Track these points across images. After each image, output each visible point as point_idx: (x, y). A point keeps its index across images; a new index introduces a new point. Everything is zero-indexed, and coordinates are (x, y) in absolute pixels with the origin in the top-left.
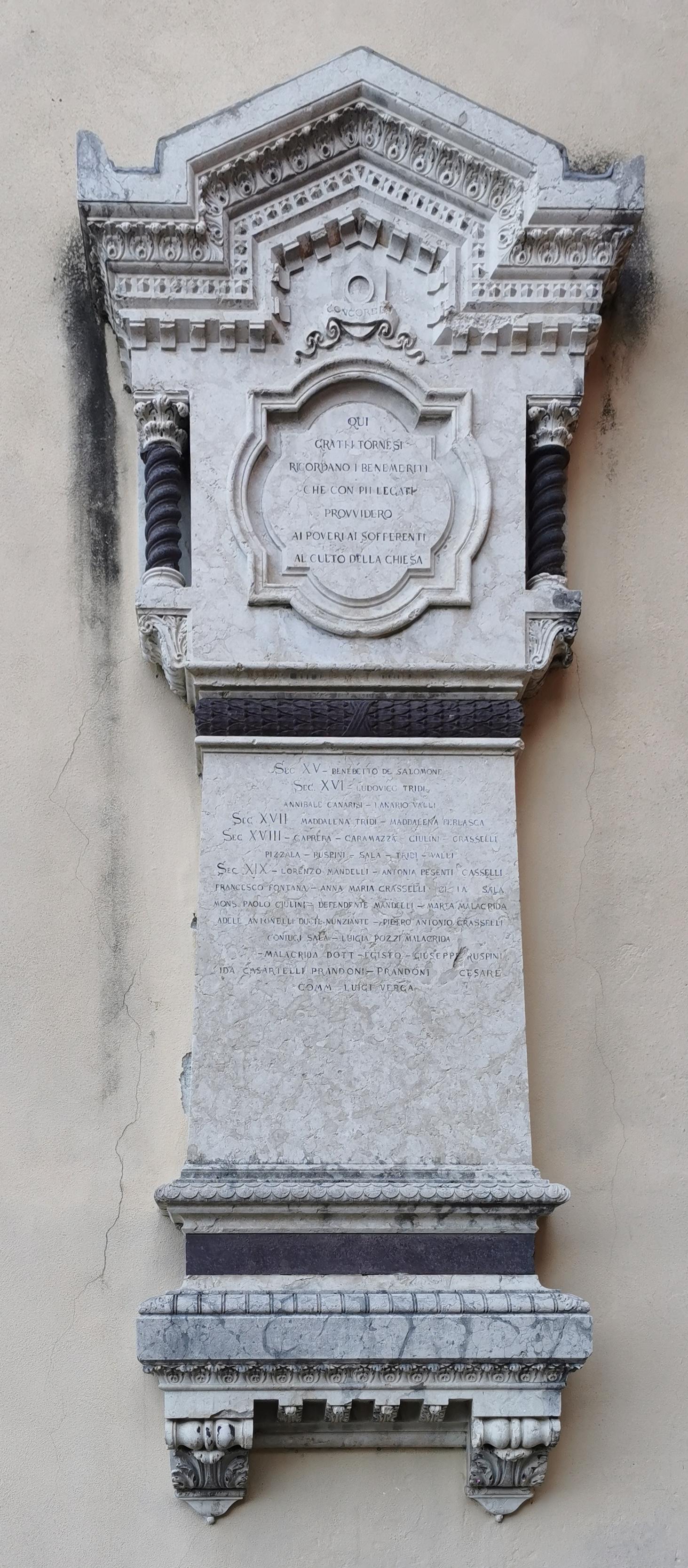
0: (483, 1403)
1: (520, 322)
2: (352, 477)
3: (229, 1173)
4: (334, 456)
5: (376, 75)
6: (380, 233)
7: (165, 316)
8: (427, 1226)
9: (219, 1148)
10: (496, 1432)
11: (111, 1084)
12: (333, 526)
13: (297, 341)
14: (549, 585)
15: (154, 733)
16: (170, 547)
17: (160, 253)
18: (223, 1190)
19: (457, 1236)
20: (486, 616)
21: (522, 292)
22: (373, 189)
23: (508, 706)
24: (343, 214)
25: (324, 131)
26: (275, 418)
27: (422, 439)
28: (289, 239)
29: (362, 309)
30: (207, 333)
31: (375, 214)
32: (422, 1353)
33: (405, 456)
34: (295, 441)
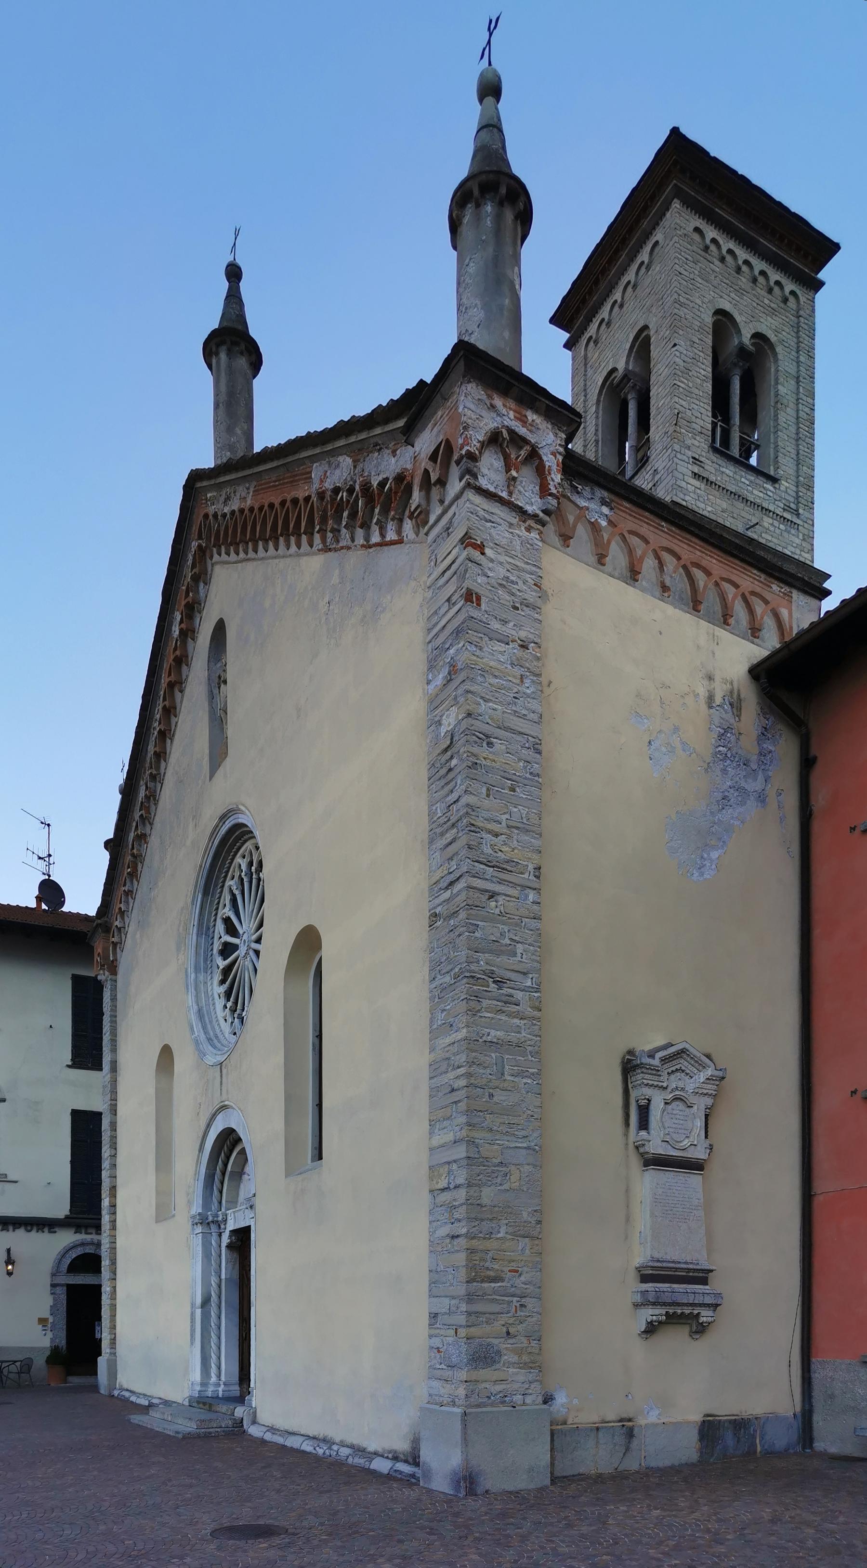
0: (703, 1313)
1: (705, 1092)
2: (678, 1117)
3: (658, 1261)
4: (674, 1112)
5: (687, 1046)
6: (683, 1071)
7: (651, 1082)
8: (691, 1274)
9: (657, 1255)
10: (705, 1319)
11: (626, 1238)
12: (674, 1126)
13: (669, 1089)
14: (708, 1142)
15: (635, 1163)
16: (644, 1124)
17: (650, 1071)
18: (659, 1264)
19: (99, 1200)
20: (699, 1147)
21: (705, 1086)
22: (683, 1063)
23: (491, 1096)
24: (678, 1067)
25: (678, 1054)
26: (666, 1103)
27: (688, 1110)
28: (670, 1070)
29: (681, 1084)
30: (657, 1086)
31: (683, 1068)
32: (696, 1302)
33: (685, 1114)
34: (670, 1107)
